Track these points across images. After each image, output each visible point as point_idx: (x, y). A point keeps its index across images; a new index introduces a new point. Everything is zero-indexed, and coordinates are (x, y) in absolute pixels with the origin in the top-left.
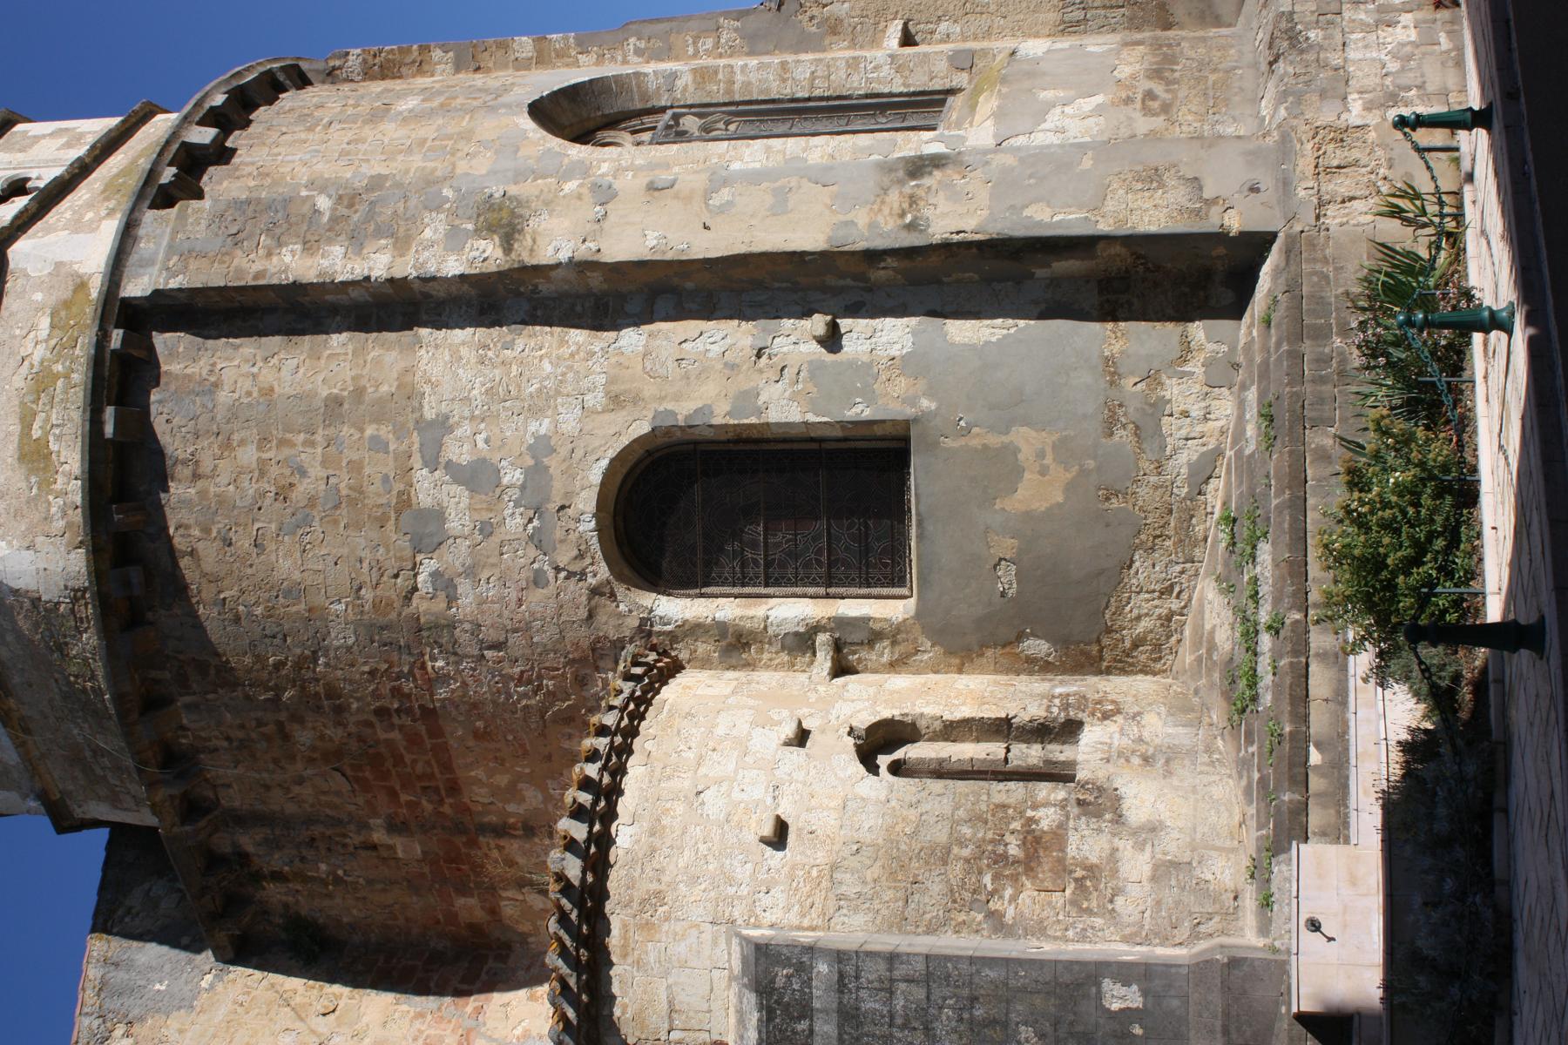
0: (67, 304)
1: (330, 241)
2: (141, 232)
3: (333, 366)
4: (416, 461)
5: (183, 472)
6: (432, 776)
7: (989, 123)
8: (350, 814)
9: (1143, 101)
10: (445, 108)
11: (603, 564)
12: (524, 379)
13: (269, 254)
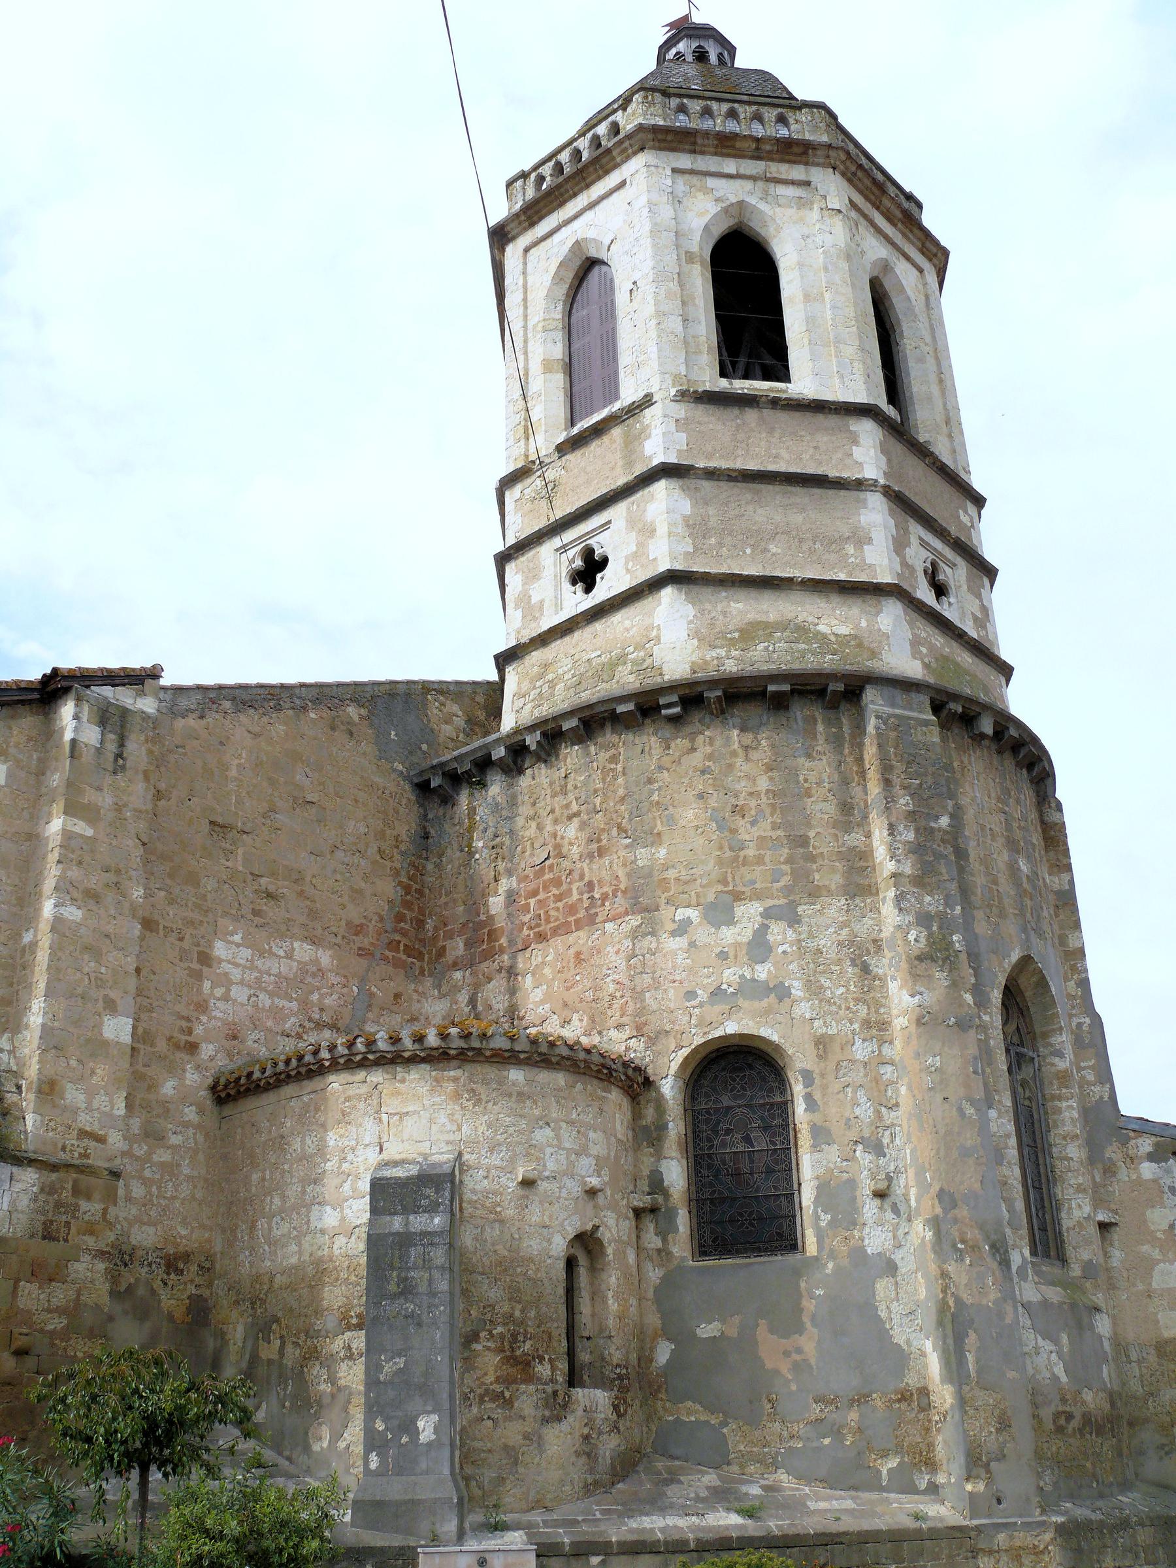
0: (860, 645)
1: (917, 830)
2: (913, 695)
3: (829, 838)
4: (770, 903)
5: (748, 738)
6: (548, 921)
7: (1039, 1296)
8: (518, 864)
9: (1064, 1412)
10: (1022, 894)
11: (703, 1040)
12: (829, 976)
13: (904, 788)
